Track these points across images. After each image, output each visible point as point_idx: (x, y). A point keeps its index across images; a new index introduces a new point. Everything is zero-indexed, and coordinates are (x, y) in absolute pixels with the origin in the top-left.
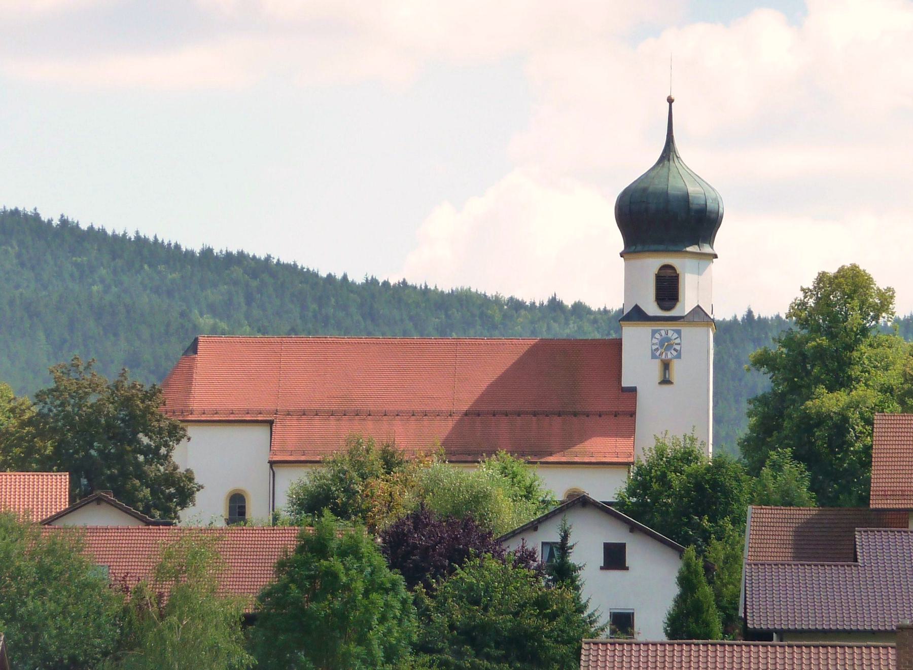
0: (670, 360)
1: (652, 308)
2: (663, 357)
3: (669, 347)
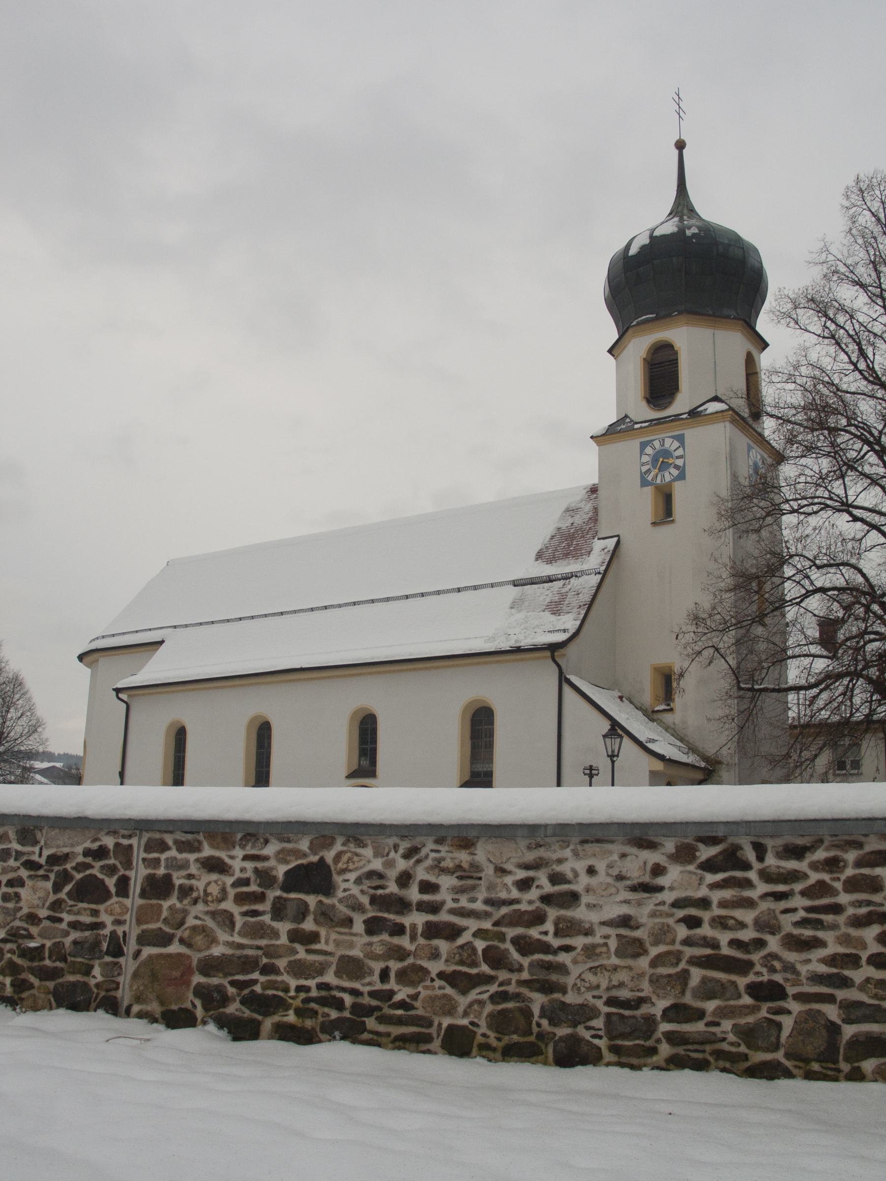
0: (669, 485)
1: (642, 412)
2: (659, 481)
3: (664, 466)
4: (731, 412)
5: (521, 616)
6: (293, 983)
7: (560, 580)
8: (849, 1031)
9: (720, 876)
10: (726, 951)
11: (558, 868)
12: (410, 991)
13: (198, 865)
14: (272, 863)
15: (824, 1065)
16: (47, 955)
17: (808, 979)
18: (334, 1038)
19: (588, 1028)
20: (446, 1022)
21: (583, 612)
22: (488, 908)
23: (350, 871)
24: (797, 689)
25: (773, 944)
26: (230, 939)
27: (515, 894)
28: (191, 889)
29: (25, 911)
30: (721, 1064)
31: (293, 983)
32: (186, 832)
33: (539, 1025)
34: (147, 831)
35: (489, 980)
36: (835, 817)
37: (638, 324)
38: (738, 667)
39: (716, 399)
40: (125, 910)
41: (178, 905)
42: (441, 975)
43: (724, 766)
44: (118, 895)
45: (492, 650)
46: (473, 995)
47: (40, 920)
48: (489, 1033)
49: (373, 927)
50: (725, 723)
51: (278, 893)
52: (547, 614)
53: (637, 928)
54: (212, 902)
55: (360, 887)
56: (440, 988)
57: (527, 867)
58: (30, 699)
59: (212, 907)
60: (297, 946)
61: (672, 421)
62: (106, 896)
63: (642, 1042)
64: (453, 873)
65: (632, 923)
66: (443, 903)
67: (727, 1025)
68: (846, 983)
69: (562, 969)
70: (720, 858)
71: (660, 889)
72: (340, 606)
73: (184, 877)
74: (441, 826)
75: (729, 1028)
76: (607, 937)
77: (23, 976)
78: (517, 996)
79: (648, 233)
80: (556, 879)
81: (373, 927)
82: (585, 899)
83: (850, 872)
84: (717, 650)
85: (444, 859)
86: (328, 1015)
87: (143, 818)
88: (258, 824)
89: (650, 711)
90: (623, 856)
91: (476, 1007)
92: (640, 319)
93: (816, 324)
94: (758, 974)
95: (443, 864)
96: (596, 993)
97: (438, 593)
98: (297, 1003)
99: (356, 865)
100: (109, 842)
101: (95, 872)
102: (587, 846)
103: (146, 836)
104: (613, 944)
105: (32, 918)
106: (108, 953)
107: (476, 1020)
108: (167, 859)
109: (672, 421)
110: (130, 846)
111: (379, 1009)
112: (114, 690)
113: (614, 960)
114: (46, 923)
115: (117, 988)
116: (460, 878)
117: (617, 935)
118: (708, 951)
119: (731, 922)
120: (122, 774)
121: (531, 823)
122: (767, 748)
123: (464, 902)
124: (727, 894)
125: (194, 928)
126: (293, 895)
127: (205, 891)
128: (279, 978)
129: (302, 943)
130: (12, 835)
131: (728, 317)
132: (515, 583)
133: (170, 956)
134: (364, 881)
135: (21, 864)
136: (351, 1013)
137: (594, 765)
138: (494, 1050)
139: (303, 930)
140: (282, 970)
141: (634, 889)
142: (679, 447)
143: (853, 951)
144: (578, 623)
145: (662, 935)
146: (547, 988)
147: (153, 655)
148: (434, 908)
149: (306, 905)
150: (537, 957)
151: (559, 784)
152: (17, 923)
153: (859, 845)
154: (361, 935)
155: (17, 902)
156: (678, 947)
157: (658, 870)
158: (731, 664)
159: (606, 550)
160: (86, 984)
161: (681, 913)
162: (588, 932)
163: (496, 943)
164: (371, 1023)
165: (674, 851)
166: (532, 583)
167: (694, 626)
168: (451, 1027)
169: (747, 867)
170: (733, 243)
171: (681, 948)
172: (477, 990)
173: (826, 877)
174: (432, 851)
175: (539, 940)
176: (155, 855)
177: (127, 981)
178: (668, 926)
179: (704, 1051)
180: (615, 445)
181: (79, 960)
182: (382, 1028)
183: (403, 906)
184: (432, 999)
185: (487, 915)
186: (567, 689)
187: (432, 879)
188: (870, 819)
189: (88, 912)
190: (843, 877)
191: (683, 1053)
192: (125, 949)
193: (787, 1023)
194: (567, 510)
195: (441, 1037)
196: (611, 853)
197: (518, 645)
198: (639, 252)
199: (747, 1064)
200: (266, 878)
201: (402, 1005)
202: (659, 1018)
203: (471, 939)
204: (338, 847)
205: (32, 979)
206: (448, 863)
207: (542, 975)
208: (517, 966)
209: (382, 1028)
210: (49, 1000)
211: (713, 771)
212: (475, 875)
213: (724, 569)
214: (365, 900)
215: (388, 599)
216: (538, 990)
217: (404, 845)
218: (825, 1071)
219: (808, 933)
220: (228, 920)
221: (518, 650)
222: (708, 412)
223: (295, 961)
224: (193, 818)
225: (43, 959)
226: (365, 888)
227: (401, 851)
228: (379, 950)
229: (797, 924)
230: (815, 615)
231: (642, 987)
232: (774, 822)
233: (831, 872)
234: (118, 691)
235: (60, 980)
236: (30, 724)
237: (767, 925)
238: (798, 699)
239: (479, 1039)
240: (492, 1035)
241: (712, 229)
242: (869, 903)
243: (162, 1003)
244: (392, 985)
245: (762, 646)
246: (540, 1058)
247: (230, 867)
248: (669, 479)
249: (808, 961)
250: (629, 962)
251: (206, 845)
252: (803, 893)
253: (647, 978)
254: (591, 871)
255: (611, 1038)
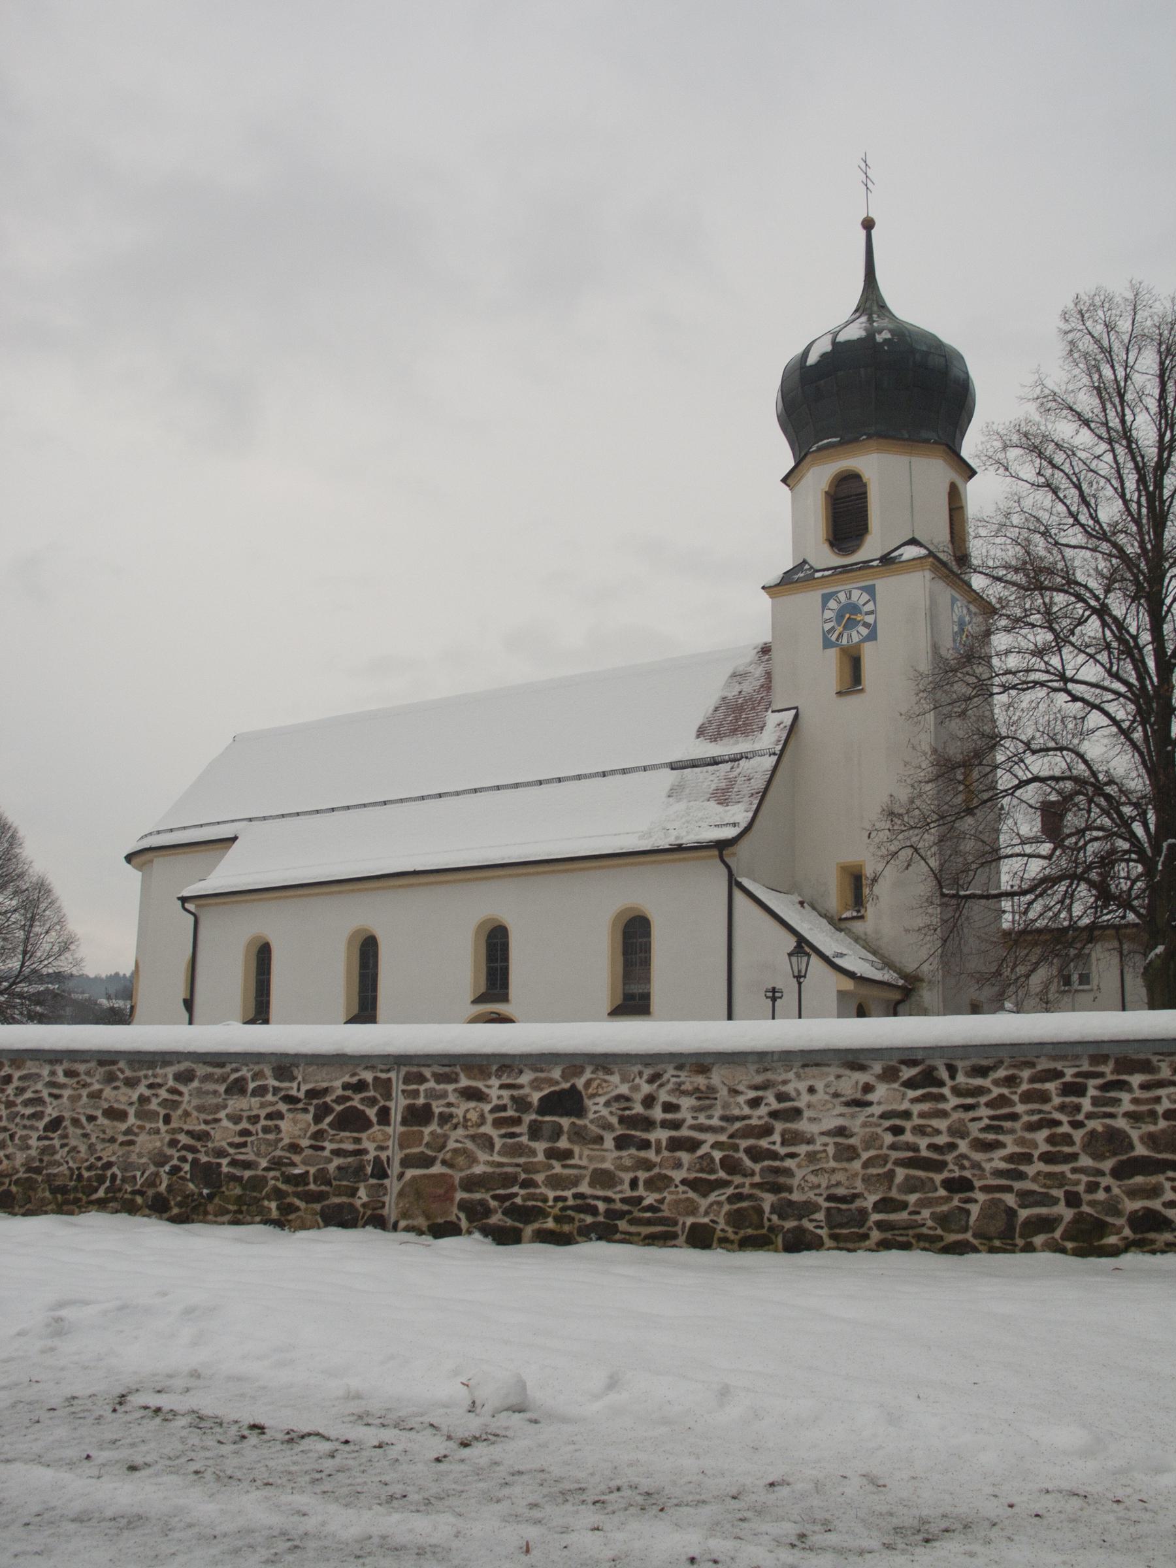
0: (857, 646)
1: (824, 557)
2: (844, 641)
3: (851, 624)
4: (931, 559)
5: (681, 806)
6: (551, 1195)
7: (727, 762)
8: (1024, 1214)
9: (919, 1092)
10: (924, 1153)
11: (783, 1089)
12: (657, 1196)
13: (457, 1095)
14: (527, 1090)
15: (1004, 1241)
16: (311, 1179)
17: (991, 1174)
18: (591, 1239)
19: (811, 1221)
20: (690, 1221)
21: (756, 802)
22: (723, 1124)
23: (600, 1095)
24: (1010, 895)
25: (963, 1146)
26: (490, 1159)
27: (747, 1111)
28: (451, 1116)
29: (286, 1141)
30: (922, 1244)
31: (551, 1195)
32: (443, 1066)
33: (769, 1220)
34: (405, 1065)
35: (725, 1184)
36: (1013, 1042)
37: (820, 449)
38: (941, 871)
39: (913, 542)
40: (387, 1137)
41: (439, 1131)
42: (684, 1182)
43: (925, 984)
44: (379, 1123)
45: (648, 848)
46: (713, 1197)
47: (302, 1149)
48: (727, 1228)
49: (622, 1143)
50: (925, 935)
51: (534, 1117)
52: (712, 804)
53: (851, 1136)
54: (472, 1126)
55: (609, 1109)
56: (684, 1192)
57: (756, 1088)
58: (59, 909)
59: (472, 1131)
60: (554, 1162)
61: (860, 569)
62: (366, 1124)
63: (856, 1230)
64: (692, 1095)
65: (847, 1133)
66: (684, 1121)
67: (926, 1213)
68: (1021, 1176)
69: (788, 1172)
70: (919, 1077)
71: (870, 1104)
72: (457, 793)
73: (443, 1106)
74: (681, 1055)
75: (928, 1216)
76: (826, 1145)
77: (289, 1200)
78: (750, 1197)
79: (830, 337)
80: (781, 1097)
81: (622, 1143)
82: (807, 1114)
83: (1025, 1087)
84: (916, 850)
85: (684, 1083)
86: (584, 1220)
87: (402, 1053)
88: (514, 1056)
89: (836, 918)
90: (839, 1077)
91: (715, 1207)
92: (820, 443)
93: (1028, 471)
94: (951, 1171)
95: (683, 1087)
96: (817, 1191)
97: (579, 777)
98: (556, 1211)
99: (605, 1090)
100: (368, 1076)
101: (356, 1103)
102: (807, 1069)
103: (404, 1070)
104: (831, 1150)
105: (294, 1148)
106: (373, 1176)
107: (715, 1218)
108: (426, 1090)
109: (860, 569)
110: (389, 1079)
111: (630, 1212)
112: (179, 898)
113: (832, 1164)
114: (309, 1152)
115: (383, 1206)
116: (699, 1099)
117: (835, 1143)
118: (910, 1154)
119: (929, 1129)
120: (189, 1004)
121: (760, 1050)
122: (975, 964)
123: (702, 1120)
124: (925, 1107)
125: (455, 1151)
126: (547, 1118)
127: (464, 1117)
128: (538, 1191)
129: (558, 1159)
130: (268, 1072)
131: (927, 441)
132: (674, 766)
133: (433, 1176)
134: (613, 1104)
135: (280, 1099)
136: (605, 1217)
137: (778, 986)
138: (732, 1242)
139: (558, 1148)
140: (540, 1183)
141: (848, 1104)
142: (869, 600)
143: (1027, 1150)
144: (750, 814)
145: (871, 1141)
146: (776, 1189)
147: (224, 855)
148: (676, 1125)
149: (560, 1126)
150: (766, 1163)
151: (773, 1018)
152: (278, 1153)
153: (1032, 1065)
154: (611, 1151)
155: (278, 1134)
156: (885, 1151)
157: (868, 1088)
158: (932, 865)
159: (782, 726)
160: (351, 1205)
161: (887, 1123)
162: (810, 1141)
163: (731, 1153)
164: (622, 1225)
165: (881, 1072)
166: (694, 766)
167: (889, 822)
168: (694, 1225)
169: (941, 1084)
170: (932, 351)
171: (888, 1152)
172: (716, 1193)
173: (1005, 1091)
174: (673, 1076)
175: (768, 1150)
176: (414, 1087)
177: (393, 1201)
178: (877, 1134)
179: (907, 1235)
180: (793, 597)
181: (344, 1183)
182: (633, 1229)
183: (648, 1124)
184: (677, 1202)
185: (722, 1130)
186: (738, 896)
187: (674, 1100)
188: (1040, 1044)
189: (351, 1140)
190: (1019, 1091)
191: (890, 1237)
192: (389, 1172)
193: (975, 1209)
194: (734, 675)
195: (686, 1233)
196: (828, 1074)
197: (679, 842)
198: (819, 362)
199: (942, 1244)
200: (522, 1104)
201: (650, 1208)
202: (870, 1210)
203: (709, 1150)
204: (588, 1074)
205: (297, 1202)
206: (687, 1087)
207: (771, 1178)
208: (750, 1172)
209: (633, 1229)
210: (317, 1221)
211: (911, 990)
212: (711, 1096)
213: (924, 758)
214: (614, 1120)
215: (517, 786)
216: (768, 1191)
217: (648, 1072)
218: (1004, 1246)
219: (991, 1137)
220: (487, 1143)
221: (679, 848)
222: (904, 558)
223: (552, 1175)
224: (450, 1053)
225: (308, 1184)
226: (613, 1109)
227: (645, 1077)
228: (628, 1162)
229: (983, 1130)
230: (1031, 806)
231: (856, 1185)
232: (963, 1047)
233: (1009, 1087)
234: (184, 900)
235: (326, 1202)
236: (60, 940)
237: (958, 1131)
238: (1013, 906)
239: (719, 1234)
240: (730, 1230)
241: (907, 333)
242: (1040, 1112)
243: (428, 1218)
244: (641, 1191)
245: (969, 845)
246: (771, 1247)
247: (488, 1095)
248: (858, 640)
249: (991, 1160)
250: (845, 1165)
251: (462, 1076)
252: (987, 1105)
253: (860, 1177)
254: (811, 1090)
255: (831, 1228)
